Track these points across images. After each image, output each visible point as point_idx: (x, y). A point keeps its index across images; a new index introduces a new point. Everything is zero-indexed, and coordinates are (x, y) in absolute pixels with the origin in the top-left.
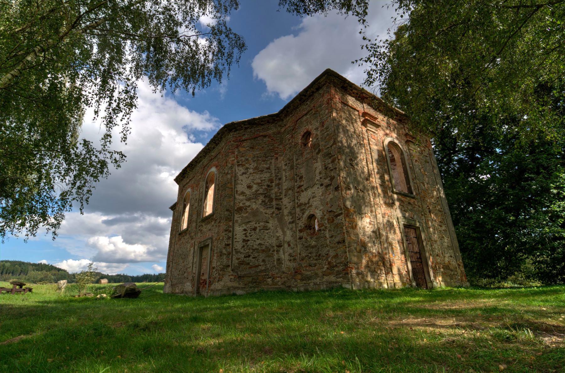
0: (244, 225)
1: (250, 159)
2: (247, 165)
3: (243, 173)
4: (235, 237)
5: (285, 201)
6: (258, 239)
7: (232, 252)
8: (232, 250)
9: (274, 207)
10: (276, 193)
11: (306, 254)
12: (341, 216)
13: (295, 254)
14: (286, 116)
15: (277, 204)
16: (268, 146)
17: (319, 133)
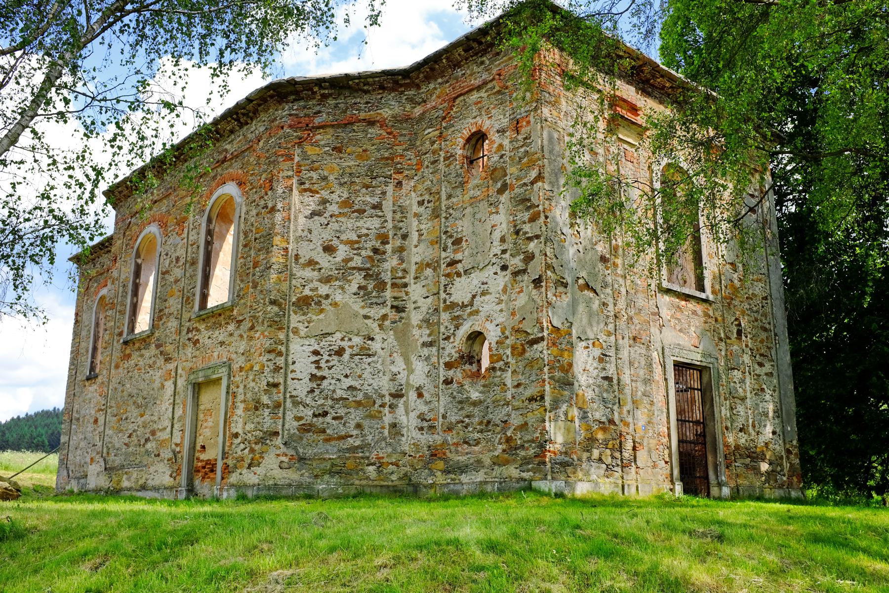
0: (313, 340)
1: (331, 178)
2: (325, 194)
3: (314, 214)
4: (291, 367)
5: (416, 291)
6: (346, 376)
7: (285, 402)
8: (285, 398)
9: (389, 304)
10: (394, 270)
11: (457, 418)
12: (541, 345)
13: (432, 417)
14: (428, 78)
15: (394, 298)
16: (378, 150)
17: (506, 142)
